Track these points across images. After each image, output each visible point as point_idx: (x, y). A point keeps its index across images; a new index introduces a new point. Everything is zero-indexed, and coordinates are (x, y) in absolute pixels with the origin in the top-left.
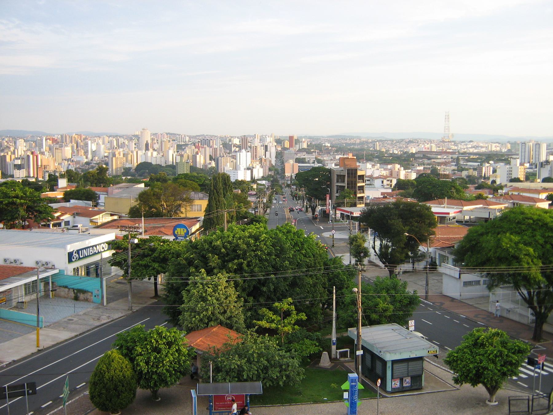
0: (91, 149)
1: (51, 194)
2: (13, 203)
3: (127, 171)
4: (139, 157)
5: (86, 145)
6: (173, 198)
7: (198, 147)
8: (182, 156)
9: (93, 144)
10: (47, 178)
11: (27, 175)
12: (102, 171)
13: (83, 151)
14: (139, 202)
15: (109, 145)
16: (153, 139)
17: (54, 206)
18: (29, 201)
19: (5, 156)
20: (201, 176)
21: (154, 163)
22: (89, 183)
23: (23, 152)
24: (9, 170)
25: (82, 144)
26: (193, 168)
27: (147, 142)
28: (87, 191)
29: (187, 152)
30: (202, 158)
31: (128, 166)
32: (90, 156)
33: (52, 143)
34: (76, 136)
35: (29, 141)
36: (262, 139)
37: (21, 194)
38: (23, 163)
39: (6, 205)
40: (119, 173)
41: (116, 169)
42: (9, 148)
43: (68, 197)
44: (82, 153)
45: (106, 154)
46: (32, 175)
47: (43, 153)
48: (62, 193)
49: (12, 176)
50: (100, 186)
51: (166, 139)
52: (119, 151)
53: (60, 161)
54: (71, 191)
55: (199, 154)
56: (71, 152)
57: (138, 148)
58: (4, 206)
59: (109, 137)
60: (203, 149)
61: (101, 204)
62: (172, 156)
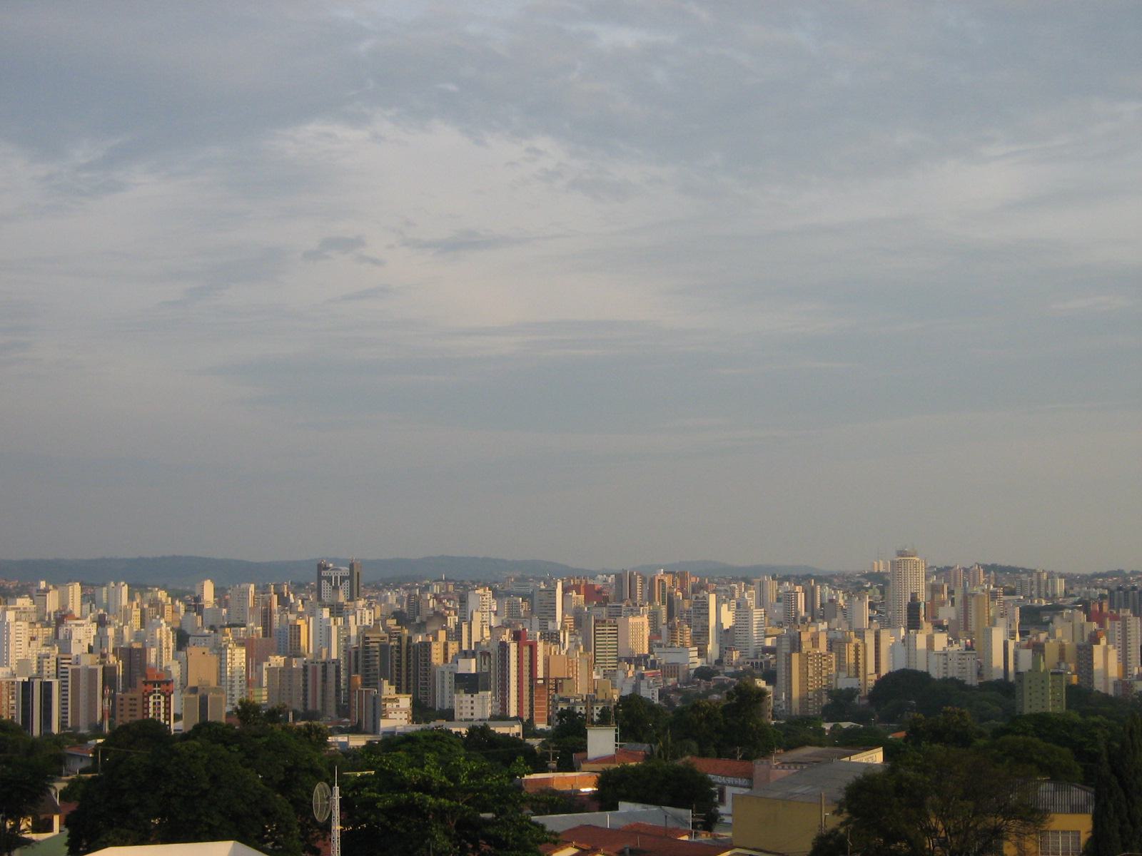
1: (560, 780)
2: (413, 809)
3: (840, 703)
4: (882, 652)
7: (1098, 617)
8: (1038, 649)
11: (498, 712)
13: (689, 632)
14: (846, 815)
15: (778, 611)
16: (934, 590)
17: (555, 822)
18: (467, 803)
19: (426, 647)
20: (1097, 725)
21: (936, 674)
23: (487, 633)
24: (438, 693)
25: (686, 605)
26: (1080, 695)
27: (914, 597)
29: (1059, 633)
30: (1113, 656)
32: (712, 648)
33: (587, 600)
35: (508, 594)
38: (485, 668)
40: (813, 710)
41: (804, 700)
42: (441, 617)
43: (613, 788)
44: (687, 639)
45: (769, 642)
46: (513, 712)
47: (552, 637)
48: (594, 777)
49: (449, 715)
50: (732, 756)
51: (983, 586)
52: (812, 630)
53: (611, 662)
54: (624, 770)
55: (1103, 641)
56: (647, 632)
57: (881, 620)
58: (382, 819)
59: (781, 581)
60: (1117, 624)
62: (1002, 647)
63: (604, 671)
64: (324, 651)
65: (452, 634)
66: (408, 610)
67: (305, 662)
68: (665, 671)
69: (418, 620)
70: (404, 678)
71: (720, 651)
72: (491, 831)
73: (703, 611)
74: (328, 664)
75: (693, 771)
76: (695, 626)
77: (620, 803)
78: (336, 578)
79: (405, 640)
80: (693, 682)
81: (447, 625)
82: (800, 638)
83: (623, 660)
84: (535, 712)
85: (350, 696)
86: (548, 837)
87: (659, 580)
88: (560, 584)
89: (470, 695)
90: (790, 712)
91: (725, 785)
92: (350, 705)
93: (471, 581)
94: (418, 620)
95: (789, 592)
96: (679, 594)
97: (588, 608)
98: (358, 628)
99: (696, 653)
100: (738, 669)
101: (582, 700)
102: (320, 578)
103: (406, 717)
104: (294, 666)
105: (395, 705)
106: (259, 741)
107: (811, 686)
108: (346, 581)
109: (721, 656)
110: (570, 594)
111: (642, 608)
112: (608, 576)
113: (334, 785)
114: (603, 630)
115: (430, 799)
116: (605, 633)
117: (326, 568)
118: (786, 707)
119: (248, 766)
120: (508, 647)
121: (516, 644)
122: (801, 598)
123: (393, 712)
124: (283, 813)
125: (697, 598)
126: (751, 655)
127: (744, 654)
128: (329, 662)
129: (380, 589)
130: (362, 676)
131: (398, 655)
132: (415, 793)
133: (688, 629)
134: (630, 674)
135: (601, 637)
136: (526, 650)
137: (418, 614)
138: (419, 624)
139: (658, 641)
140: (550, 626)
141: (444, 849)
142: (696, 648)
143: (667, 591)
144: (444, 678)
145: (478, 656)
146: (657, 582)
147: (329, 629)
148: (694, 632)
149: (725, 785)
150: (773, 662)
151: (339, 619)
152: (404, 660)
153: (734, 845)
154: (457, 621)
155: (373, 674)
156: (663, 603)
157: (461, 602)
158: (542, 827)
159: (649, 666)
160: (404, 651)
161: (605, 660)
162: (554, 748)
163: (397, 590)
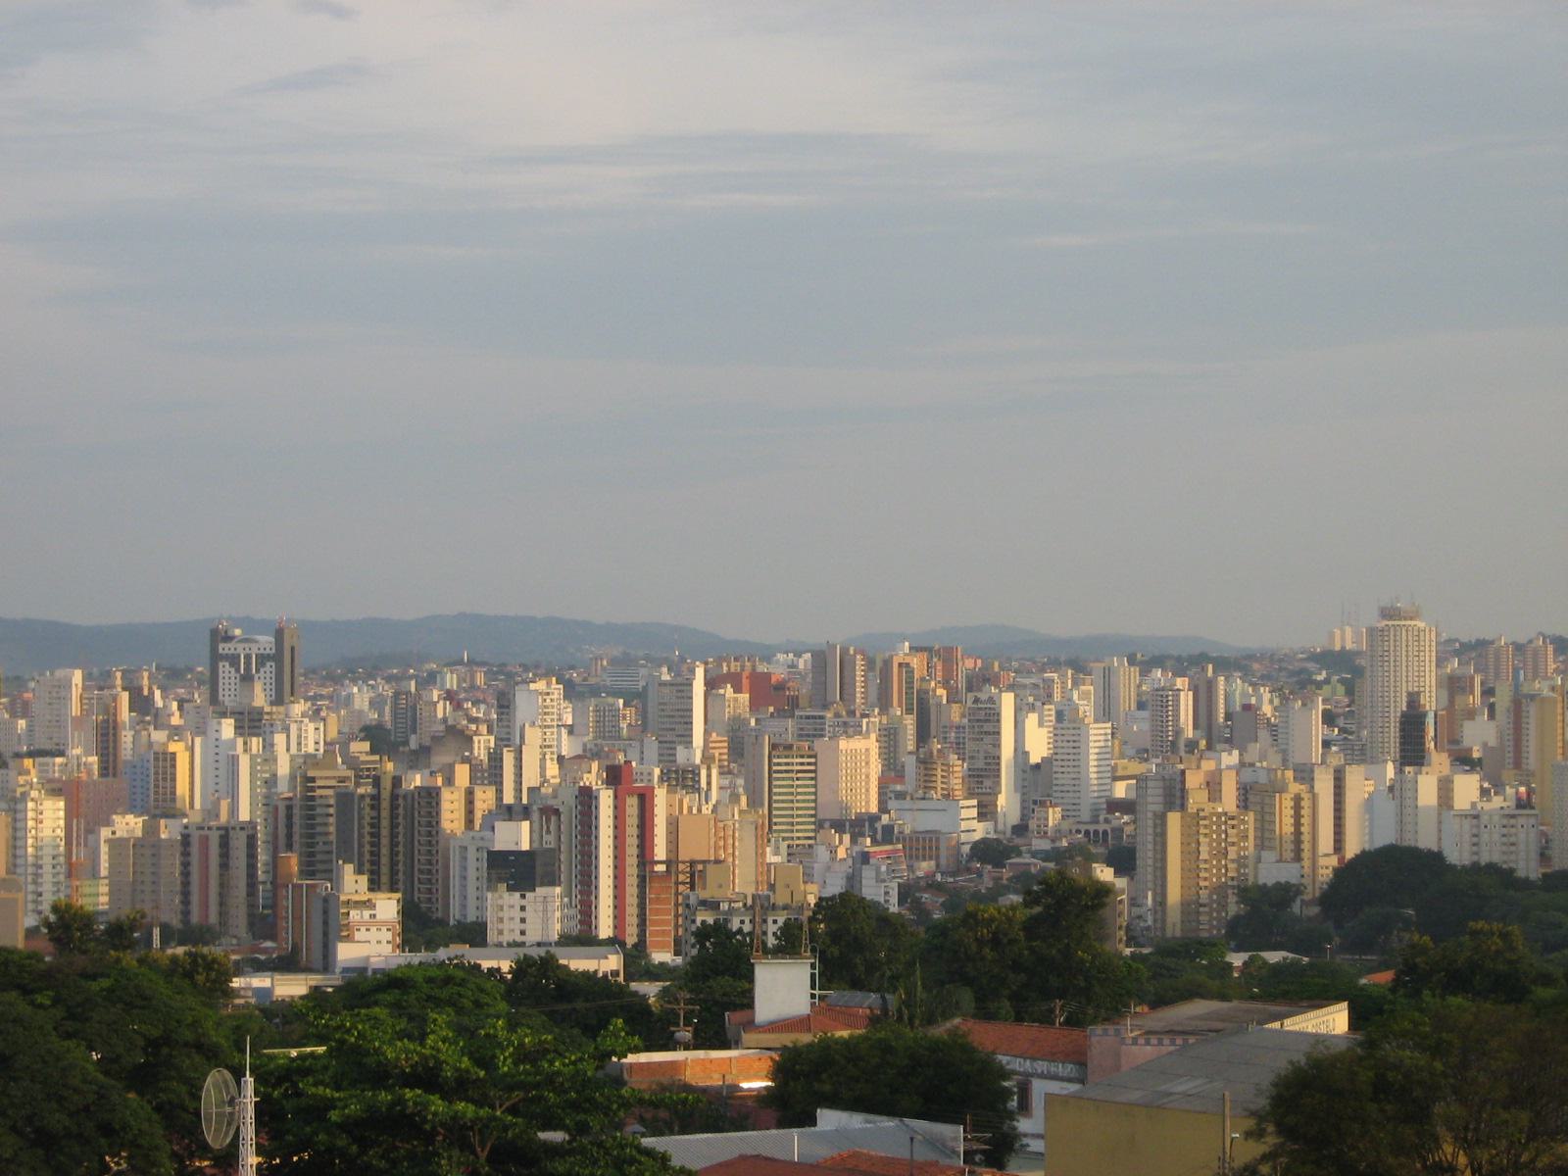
0: (1021, 753)
1: (699, 1066)
2: (402, 1123)
3: (1263, 912)
4: (1348, 811)
5: (987, 721)
6: (1525, 1117)
11: (575, 928)
12: (1065, 905)
13: (959, 768)
14: (1272, 1139)
15: (1140, 726)
18: (513, 1110)
19: (431, 796)
21: (1457, 855)
22: (966, 997)
23: (552, 769)
27: (1413, 700)
31: (1272, 872)
32: (1007, 801)
33: (755, 705)
34: (917, 662)
35: (595, 691)
37: (455, 1060)
38: (550, 841)
39: (348, 1127)
40: (1209, 927)
43: (805, 1083)
44: (956, 783)
45: (1120, 790)
47: (683, 779)
49: (475, 934)
50: (1046, 1019)
52: (1208, 765)
53: (804, 830)
56: (875, 768)
58: (342, 1141)
59: (1146, 667)
67: (186, 827)
68: (911, 849)
69: (413, 744)
71: (1023, 808)
73: (987, 727)
74: (231, 833)
75: (967, 1050)
78: (248, 657)
79: (387, 784)
80: (969, 870)
81: (472, 753)
82: (1183, 782)
83: (827, 825)
85: (275, 895)
87: (900, 665)
88: (700, 672)
90: (1163, 929)
92: (275, 915)
94: (413, 744)
95: (1163, 689)
98: (293, 759)
99: (974, 812)
100: (1058, 844)
101: (745, 905)
102: (215, 658)
103: (390, 939)
105: (366, 914)
106: (94, 986)
107: (1205, 879)
108: (268, 664)
109: (1024, 817)
110: (722, 691)
111: (865, 721)
112: (798, 655)
113: (245, 1076)
114: (787, 764)
116: (792, 771)
117: (228, 638)
118: (1155, 921)
119: (68, 1036)
121: (611, 792)
122: (1186, 701)
123: (363, 929)
125: (976, 700)
126: (1086, 816)
128: (234, 828)
130: (301, 854)
131: (374, 813)
132: (407, 1090)
133: (960, 762)
134: (841, 853)
135: (783, 779)
136: (632, 804)
138: (414, 752)
139: (898, 788)
142: (974, 802)
143: (916, 686)
145: (536, 816)
147: (234, 761)
150: (1128, 830)
151: (254, 739)
152: (385, 823)
154: (492, 745)
156: (909, 711)
157: (500, 706)
159: (879, 836)
160: (385, 804)
161: (792, 824)
163: (371, 682)
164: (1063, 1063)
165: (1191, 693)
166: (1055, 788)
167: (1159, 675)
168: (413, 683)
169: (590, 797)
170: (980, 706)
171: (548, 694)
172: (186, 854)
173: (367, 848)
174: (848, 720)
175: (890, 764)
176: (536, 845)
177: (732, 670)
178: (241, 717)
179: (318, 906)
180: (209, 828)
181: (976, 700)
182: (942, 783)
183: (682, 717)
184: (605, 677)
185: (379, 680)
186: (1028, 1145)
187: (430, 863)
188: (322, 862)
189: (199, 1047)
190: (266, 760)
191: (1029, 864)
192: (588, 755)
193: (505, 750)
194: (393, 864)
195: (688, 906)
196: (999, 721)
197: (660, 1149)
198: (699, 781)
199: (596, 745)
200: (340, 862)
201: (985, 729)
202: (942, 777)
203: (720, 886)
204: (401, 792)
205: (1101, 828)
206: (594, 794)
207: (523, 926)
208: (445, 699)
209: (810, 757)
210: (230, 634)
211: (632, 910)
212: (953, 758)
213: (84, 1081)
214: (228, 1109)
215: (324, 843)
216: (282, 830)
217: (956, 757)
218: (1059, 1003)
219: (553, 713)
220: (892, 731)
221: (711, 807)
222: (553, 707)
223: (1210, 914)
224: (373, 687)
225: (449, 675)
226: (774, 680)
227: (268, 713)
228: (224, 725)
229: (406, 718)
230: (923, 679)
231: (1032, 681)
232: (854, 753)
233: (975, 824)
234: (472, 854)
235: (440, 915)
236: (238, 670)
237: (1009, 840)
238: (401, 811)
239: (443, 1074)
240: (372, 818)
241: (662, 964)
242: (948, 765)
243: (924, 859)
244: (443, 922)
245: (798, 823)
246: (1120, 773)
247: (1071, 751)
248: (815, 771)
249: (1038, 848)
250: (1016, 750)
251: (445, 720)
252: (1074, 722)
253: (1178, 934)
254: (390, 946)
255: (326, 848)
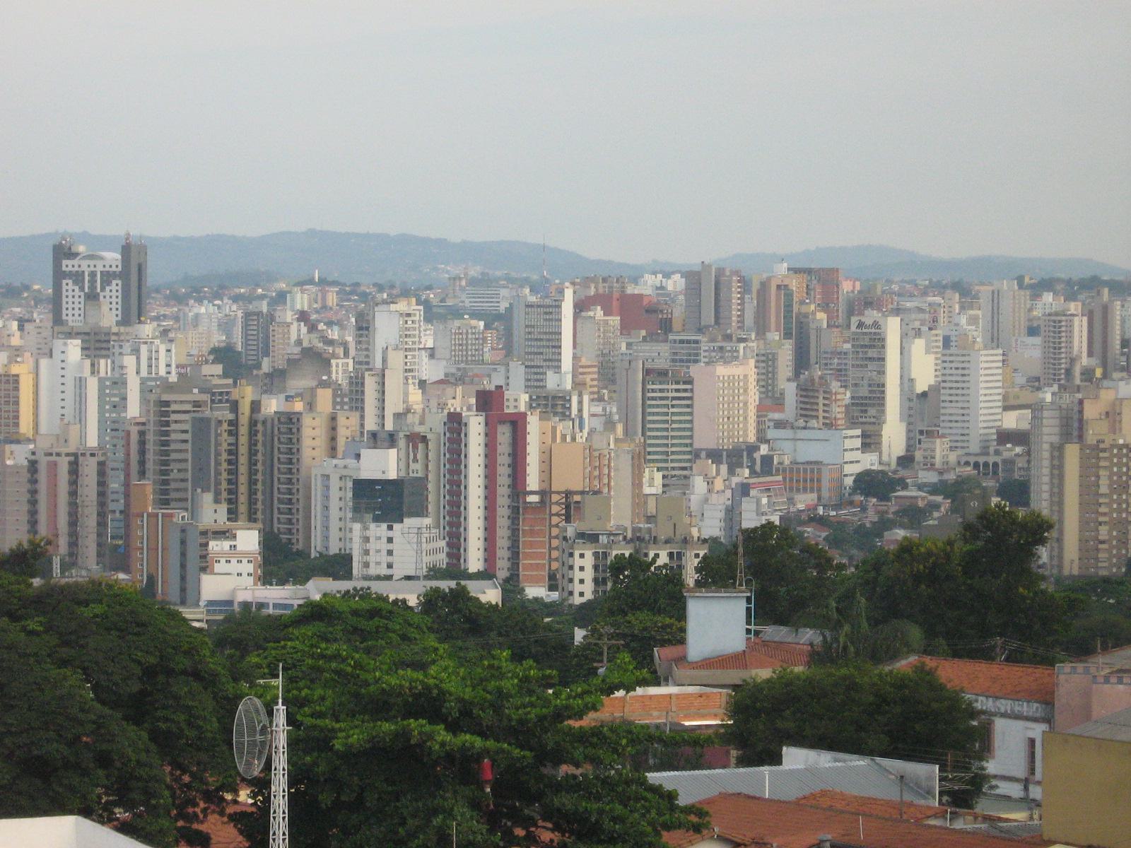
0: (907, 381)
9: (918, 345)
10: (584, 588)
11: (442, 559)
15: (1032, 351)
19: (290, 422)
23: (416, 396)
28: (901, 683)
32: (894, 435)
33: (626, 328)
35: (457, 313)
36: (968, 415)
38: (417, 469)
42: (317, 359)
43: (760, 726)
45: (1011, 421)
46: (475, 562)
48: (721, 696)
56: (754, 397)
61: (1005, 788)
63: (664, 477)
64: (74, 430)
65: (343, 396)
66: (246, 343)
67: (34, 453)
68: (791, 480)
69: (266, 366)
70: (243, 489)
71: (909, 439)
72: (565, 801)
73: (872, 353)
74: (81, 459)
75: (936, 687)
76: (856, 385)
77: (784, 748)
78: (93, 274)
79: (245, 408)
80: (851, 503)
81: (330, 377)
82: (1081, 412)
83: (703, 454)
84: (524, 562)
85: (127, 526)
86: (682, 816)
87: (779, 287)
88: (569, 295)
89: (384, 526)
90: (1060, 566)
91: (995, 714)
92: (127, 545)
93: (375, 285)
94: (266, 366)
95: (1057, 314)
96: (821, 316)
97: (629, 345)
98: (143, 382)
99: (858, 443)
100: (946, 477)
101: (625, 538)
102: (59, 276)
103: (252, 571)
104: (9, 462)
105: (226, 545)
106: (87, 612)
107: (1105, 514)
108: (114, 282)
109: (910, 447)
110: (591, 314)
111: (742, 345)
112: (667, 275)
113: (277, 704)
114: (661, 391)
115: (442, 734)
116: (667, 398)
117: (72, 255)
118: (1051, 558)
119: (64, 663)
120: (466, 424)
121: (481, 419)
122: (1080, 327)
123: (223, 560)
124: (138, 762)
125: (861, 325)
126: (975, 447)
127: (959, 444)
128: (83, 455)
129: (180, 300)
130: (155, 482)
131: (232, 440)
132: (412, 720)
133: (842, 390)
134: (719, 484)
135: (658, 406)
136: (504, 435)
137: (267, 354)
138: (267, 375)
139: (777, 416)
140: (551, 381)
141: (471, 837)
142: (858, 432)
143: (795, 308)
144: (328, 487)
145: (402, 443)
146: (773, 288)
147: (81, 383)
148: (853, 398)
149: (995, 714)
150: (1021, 463)
151: (102, 362)
152: (243, 450)
153: (1046, 838)
154: (351, 369)
155: (175, 480)
156: (787, 335)
157: (360, 328)
158: (671, 796)
159: (758, 468)
160: (243, 430)
161: (667, 453)
162: (611, 637)
163: (217, 302)
164: (1028, 702)
165: (1085, 319)
166: (942, 418)
167: (1051, 300)
168: (265, 303)
169: (460, 424)
170: (864, 330)
171: (409, 315)
172: (34, 481)
173: (224, 475)
174: (724, 344)
175: (768, 391)
176: (403, 474)
177: (601, 291)
178: (87, 337)
179: (175, 538)
180: (58, 455)
181: (861, 325)
182: (824, 411)
183: (549, 340)
184: (464, 297)
185: (226, 300)
186: (997, 787)
187: (290, 493)
188: (177, 490)
189: (196, 675)
190: (115, 383)
191: (916, 498)
192: (452, 380)
193: (367, 374)
194: (252, 493)
195: (565, 538)
196: (883, 347)
197: (668, 787)
198: (569, 408)
199: (459, 369)
200: (199, 490)
201: (870, 355)
202: (824, 405)
203: (599, 519)
204: (260, 417)
205: (991, 459)
206: (464, 421)
207: (390, 559)
208: (299, 320)
209: (685, 383)
210: (74, 250)
211: (503, 542)
212: (835, 386)
213: (82, 710)
214: (258, 738)
215: (179, 470)
216: (134, 457)
217: (839, 384)
218: (999, 640)
219: (414, 336)
220: (770, 357)
221: (585, 435)
222: (414, 329)
223: (1109, 551)
224: (219, 307)
225: (299, 295)
226: (645, 302)
227: (114, 334)
228: (70, 347)
229: (258, 340)
230: (802, 303)
231: (916, 304)
232: (731, 379)
233: (857, 455)
234: (335, 483)
235: (300, 546)
236: (82, 289)
237: (895, 472)
238: (260, 437)
239: (447, 705)
240: (229, 444)
241: (536, 599)
242: (830, 393)
243: (805, 490)
244: (303, 554)
245: (673, 453)
246: (1012, 402)
247: (959, 378)
248: (691, 398)
249: (925, 480)
250: (901, 377)
251: (299, 342)
252: (965, 349)
253: (1076, 572)
254: (251, 579)
255: (181, 476)
